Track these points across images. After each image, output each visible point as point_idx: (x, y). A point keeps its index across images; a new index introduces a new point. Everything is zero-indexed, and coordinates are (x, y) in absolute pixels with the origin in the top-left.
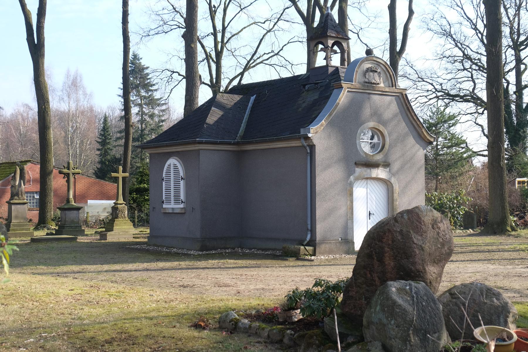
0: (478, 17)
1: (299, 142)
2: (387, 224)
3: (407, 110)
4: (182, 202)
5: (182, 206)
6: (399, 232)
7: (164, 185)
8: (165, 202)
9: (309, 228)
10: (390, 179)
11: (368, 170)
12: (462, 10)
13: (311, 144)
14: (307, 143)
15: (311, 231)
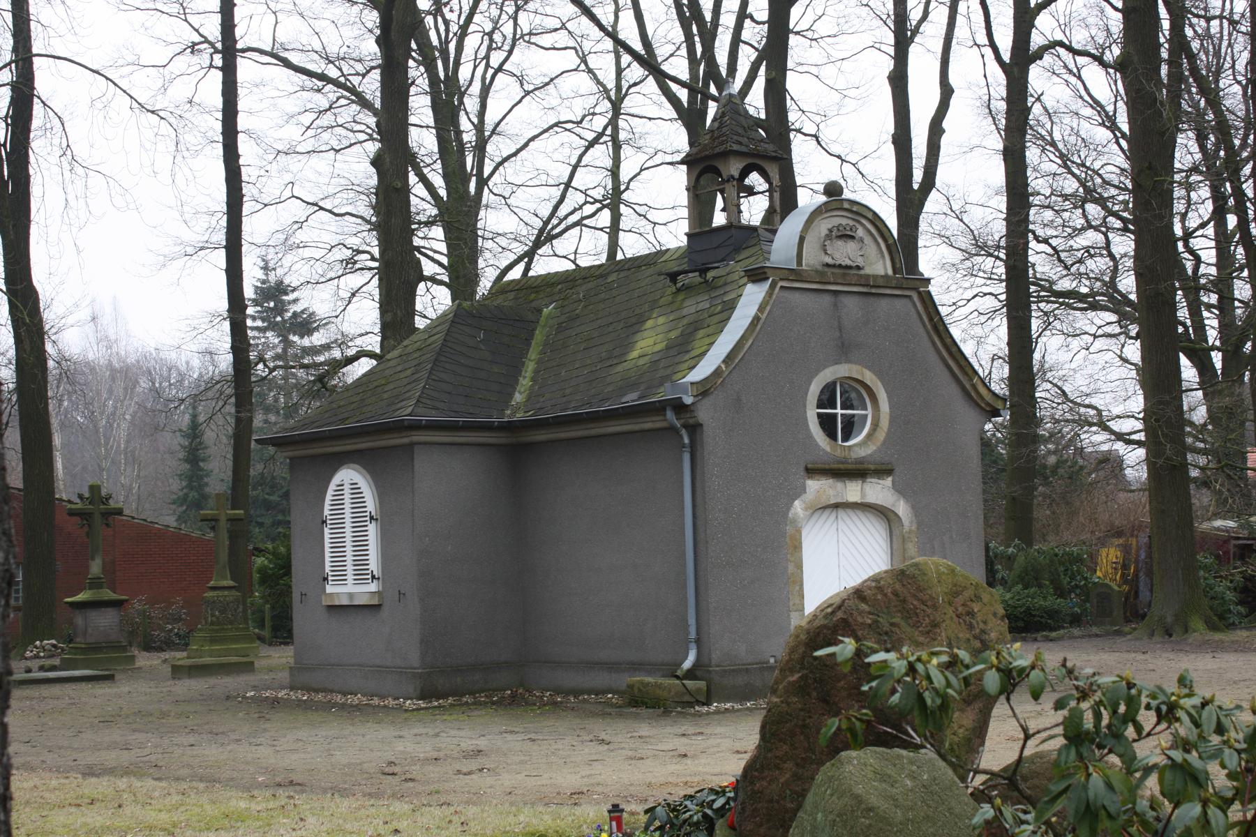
0: (1119, 98)
1: (661, 418)
2: (839, 607)
3: (932, 332)
4: (373, 577)
5: (373, 587)
6: (870, 625)
7: (327, 536)
8: (330, 578)
9: (693, 635)
10: (893, 505)
11: (839, 485)
12: (1079, 83)
13: (691, 421)
14: (683, 421)
15: (698, 641)
